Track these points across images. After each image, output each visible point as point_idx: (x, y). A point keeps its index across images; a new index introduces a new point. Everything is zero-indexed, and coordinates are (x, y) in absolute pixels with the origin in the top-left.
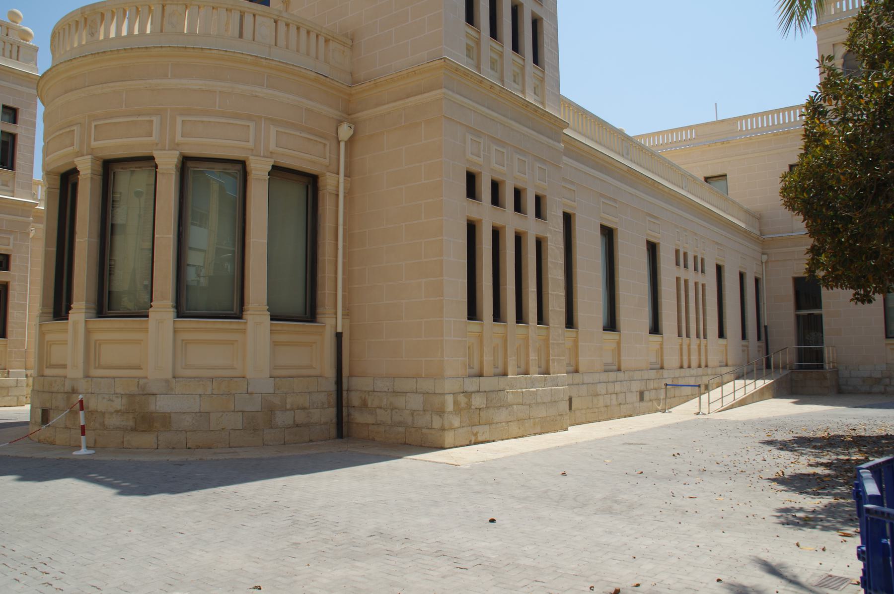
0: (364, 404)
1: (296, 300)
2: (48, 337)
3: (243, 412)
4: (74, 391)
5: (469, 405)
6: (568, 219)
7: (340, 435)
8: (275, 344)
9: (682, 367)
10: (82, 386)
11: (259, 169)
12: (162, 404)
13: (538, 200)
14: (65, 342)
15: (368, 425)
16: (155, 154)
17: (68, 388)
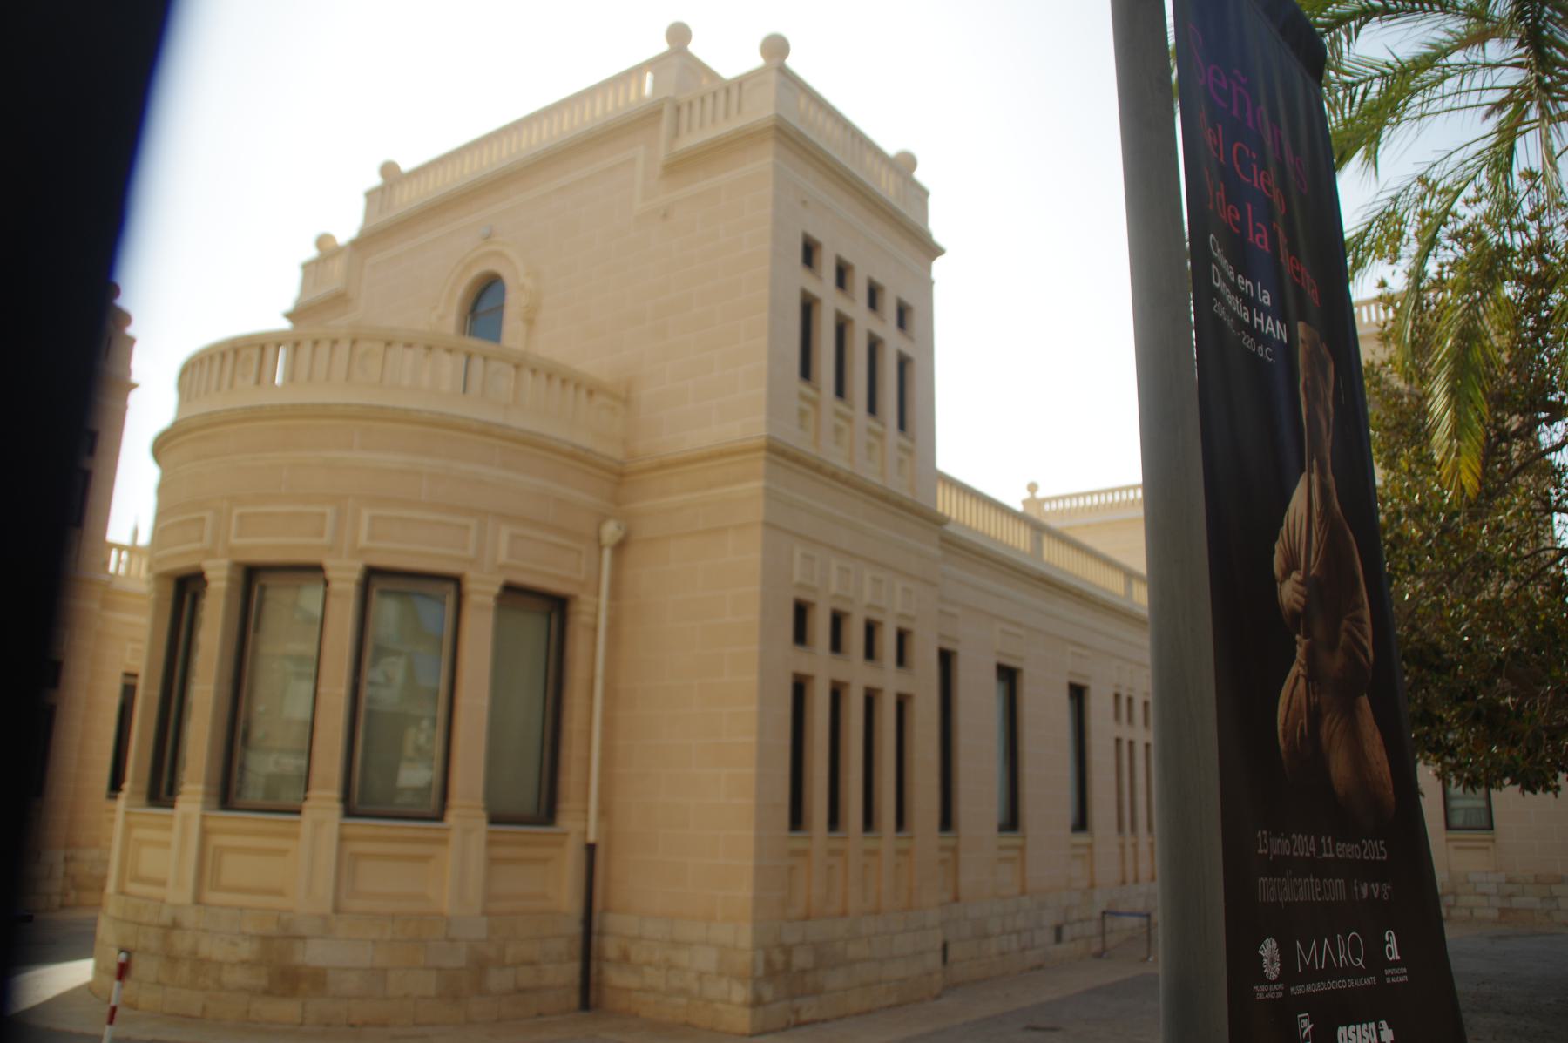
0: (625, 958)
1: (526, 798)
2: (217, 840)
3: (439, 969)
4: (176, 925)
5: (788, 964)
6: (946, 658)
7: (586, 1004)
8: (492, 861)
9: (1124, 882)
10: (190, 917)
11: (482, 593)
12: (314, 954)
13: (902, 636)
14: (166, 845)
15: (629, 990)
16: (328, 562)
17: (166, 918)
